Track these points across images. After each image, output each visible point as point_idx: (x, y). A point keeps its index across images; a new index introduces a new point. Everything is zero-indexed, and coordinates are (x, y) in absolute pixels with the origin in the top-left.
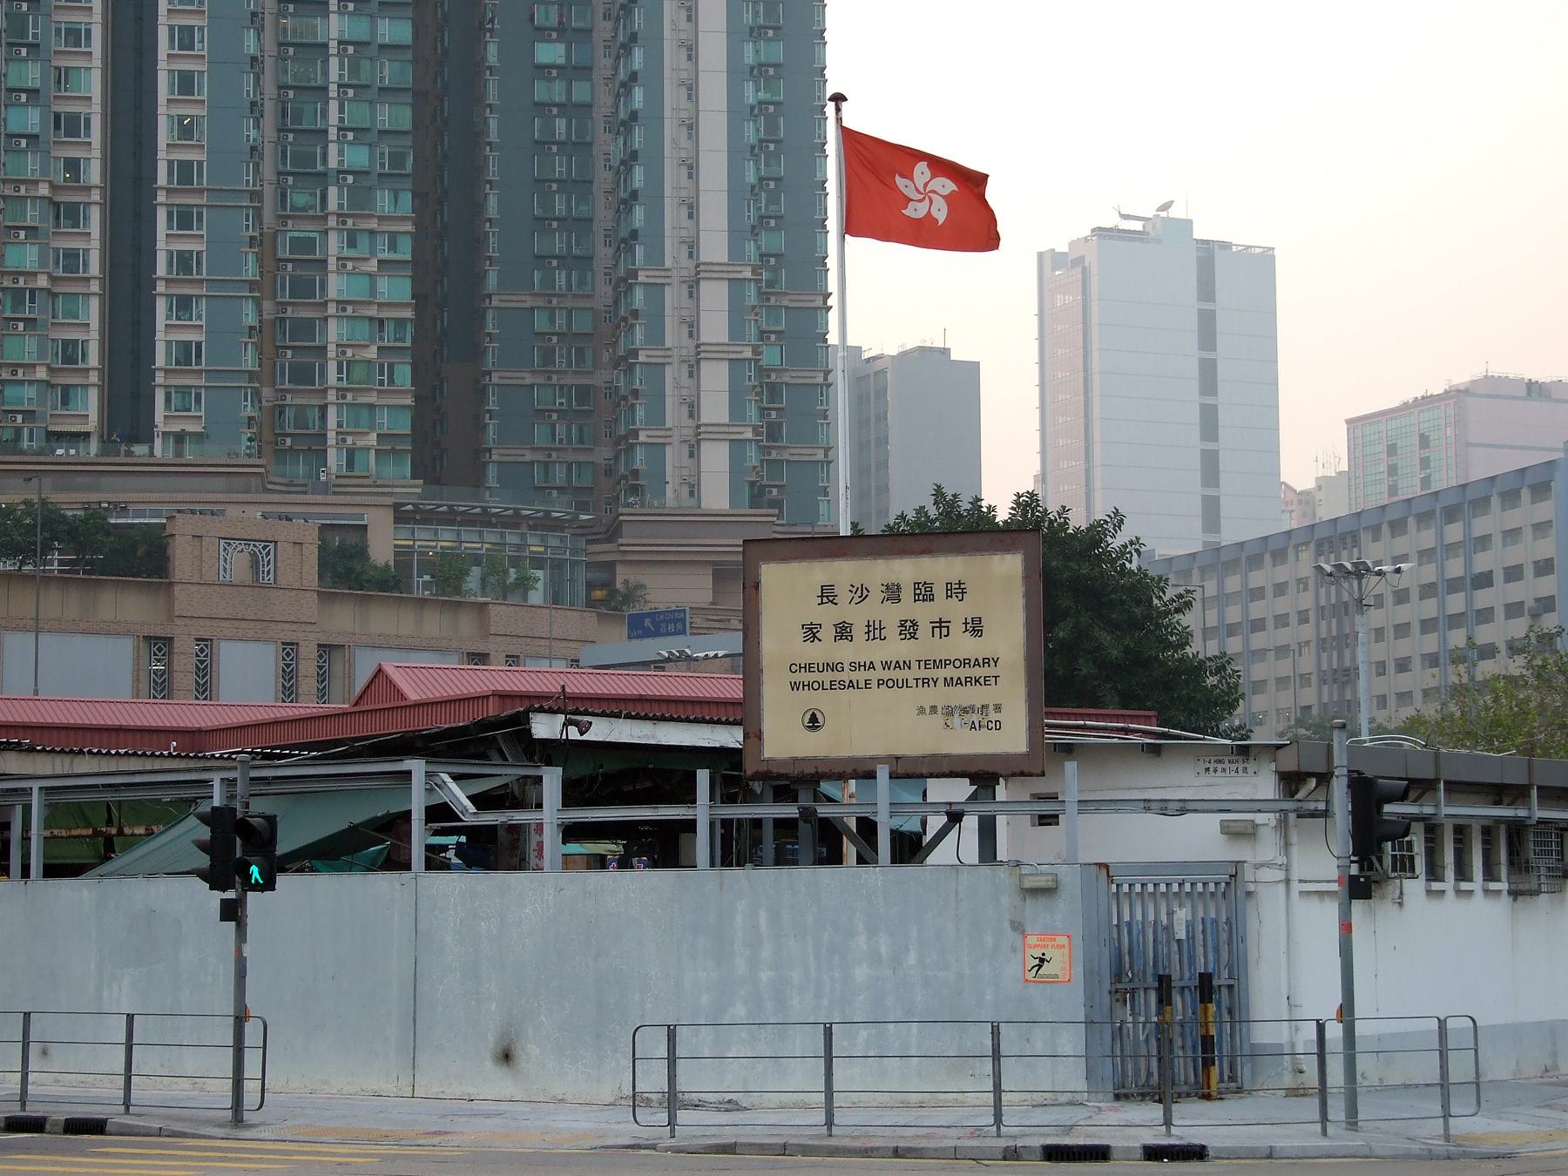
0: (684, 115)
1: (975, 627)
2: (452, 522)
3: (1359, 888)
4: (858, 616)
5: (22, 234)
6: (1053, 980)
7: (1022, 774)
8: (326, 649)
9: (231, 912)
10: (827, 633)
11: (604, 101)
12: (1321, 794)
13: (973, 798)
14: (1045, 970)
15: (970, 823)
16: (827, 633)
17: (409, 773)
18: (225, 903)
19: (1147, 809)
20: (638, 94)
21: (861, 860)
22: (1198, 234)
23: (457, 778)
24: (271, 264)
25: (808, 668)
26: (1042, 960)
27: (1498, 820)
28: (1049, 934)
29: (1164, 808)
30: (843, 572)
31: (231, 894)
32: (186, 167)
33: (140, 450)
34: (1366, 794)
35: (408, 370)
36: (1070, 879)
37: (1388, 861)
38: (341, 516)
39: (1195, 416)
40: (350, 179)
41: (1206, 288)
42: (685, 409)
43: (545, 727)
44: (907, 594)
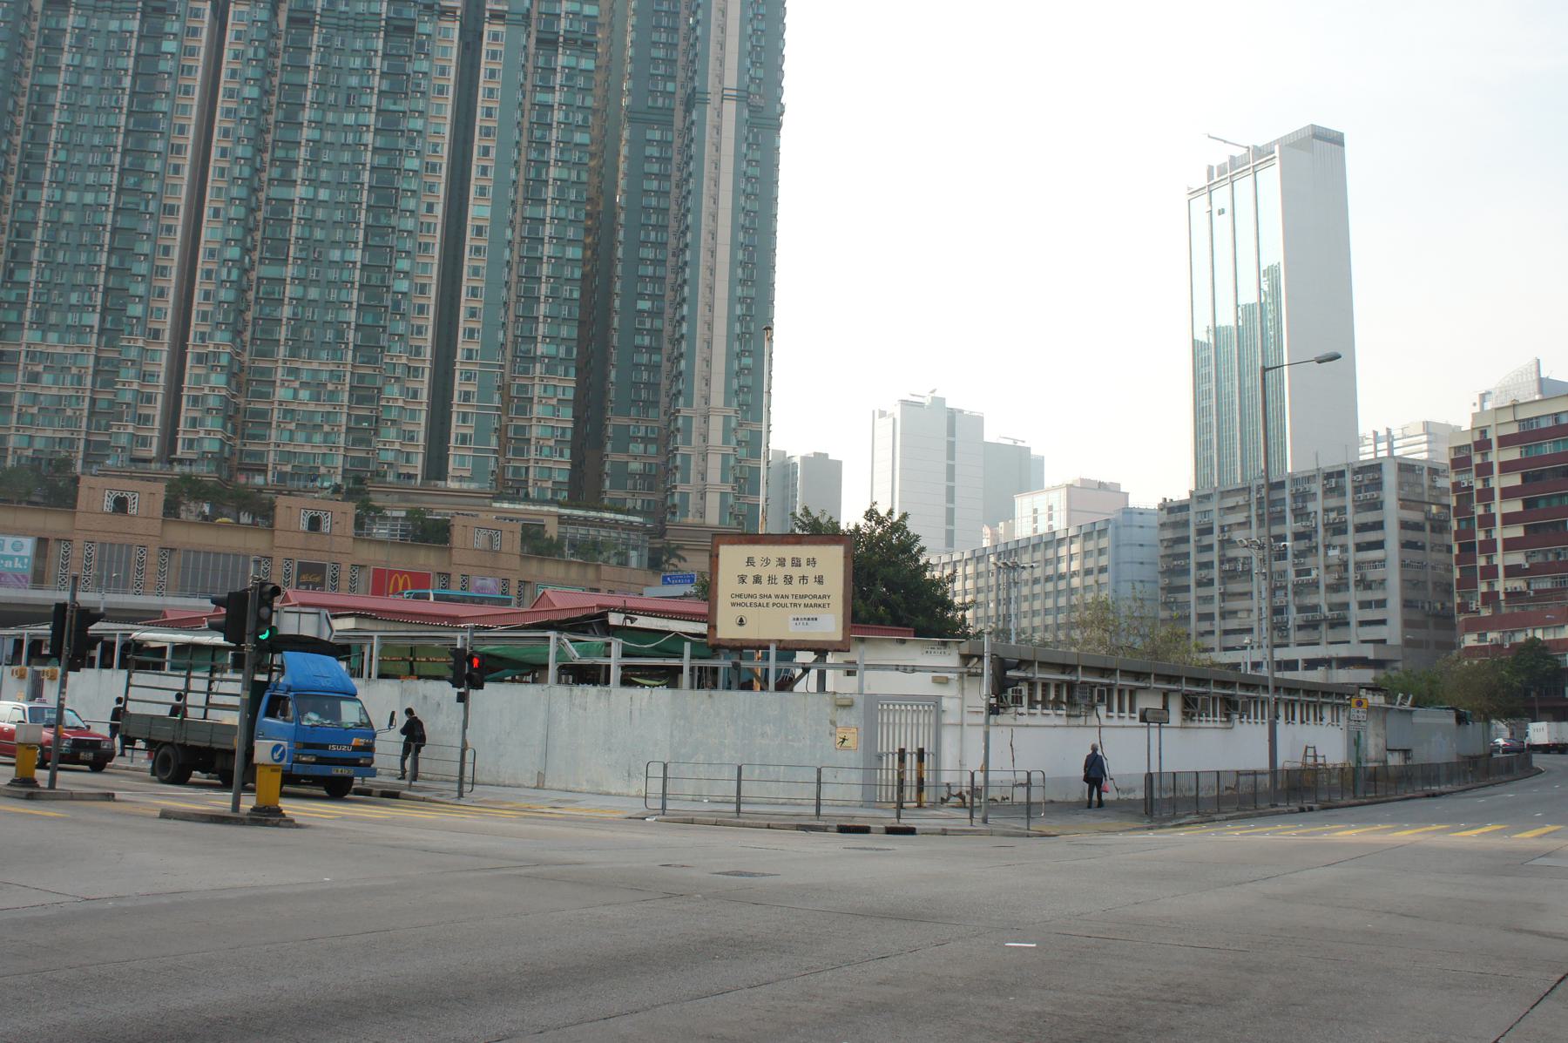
0: (706, 337)
1: (820, 580)
2: (586, 525)
3: (993, 710)
4: (765, 574)
5: (393, 380)
6: (848, 748)
7: (839, 651)
8: (523, 583)
9: (462, 698)
10: (750, 580)
11: (668, 329)
12: (979, 665)
13: (816, 661)
14: (846, 743)
15: (814, 673)
16: (750, 580)
17: (549, 638)
18: (460, 694)
19: (897, 669)
20: (685, 326)
21: (762, 689)
22: (949, 404)
23: (572, 641)
24: (507, 399)
25: (740, 596)
26: (844, 739)
27: (1063, 681)
28: (848, 727)
29: (905, 669)
30: (758, 551)
31: (462, 690)
32: (470, 351)
33: (441, 484)
34: (1001, 665)
35: (569, 451)
36: (860, 702)
37: (1010, 699)
38: (531, 520)
39: (944, 492)
40: (546, 361)
41: (951, 431)
42: (700, 477)
43: (615, 619)
44: (788, 563)
